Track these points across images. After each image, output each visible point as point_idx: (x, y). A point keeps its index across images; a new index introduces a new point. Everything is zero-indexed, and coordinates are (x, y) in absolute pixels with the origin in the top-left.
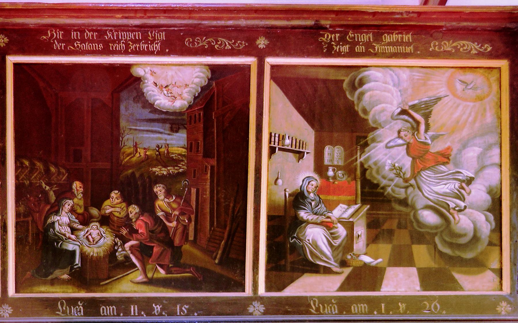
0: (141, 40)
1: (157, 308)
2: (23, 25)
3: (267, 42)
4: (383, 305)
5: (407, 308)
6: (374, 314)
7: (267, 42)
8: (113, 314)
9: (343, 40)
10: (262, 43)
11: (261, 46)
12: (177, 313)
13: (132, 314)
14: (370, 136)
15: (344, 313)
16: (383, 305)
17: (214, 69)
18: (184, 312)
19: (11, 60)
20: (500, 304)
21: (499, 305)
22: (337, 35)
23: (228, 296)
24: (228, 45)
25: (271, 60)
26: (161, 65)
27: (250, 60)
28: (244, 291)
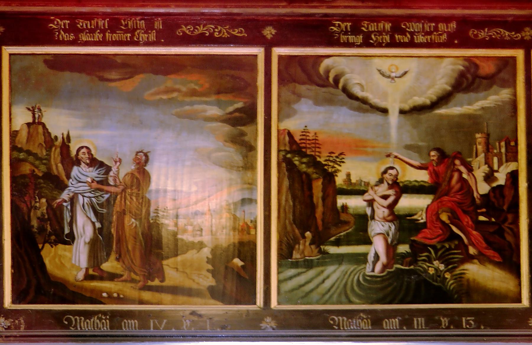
0: (107, 30)
1: (445, 321)
2: (442, 8)
3: (274, 32)
4: (165, 321)
5: (450, 323)
6: (404, 329)
7: (274, 32)
8: (396, 327)
9: (356, 30)
10: (269, 32)
11: (269, 37)
12: (462, 325)
13: (416, 327)
14: (311, 136)
15: (482, 327)
16: (165, 321)
17: (468, 59)
18: (470, 325)
19: (7, 50)
20: (265, 319)
21: (264, 321)
22: (349, 24)
23: (514, 307)
24: (226, 34)
25: (278, 51)
26: (379, 56)
27: (258, 51)
28: (255, 303)
